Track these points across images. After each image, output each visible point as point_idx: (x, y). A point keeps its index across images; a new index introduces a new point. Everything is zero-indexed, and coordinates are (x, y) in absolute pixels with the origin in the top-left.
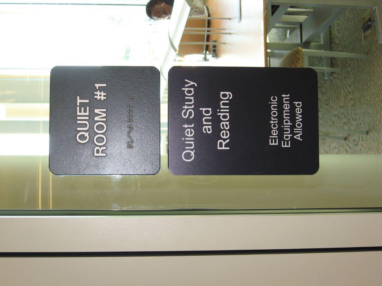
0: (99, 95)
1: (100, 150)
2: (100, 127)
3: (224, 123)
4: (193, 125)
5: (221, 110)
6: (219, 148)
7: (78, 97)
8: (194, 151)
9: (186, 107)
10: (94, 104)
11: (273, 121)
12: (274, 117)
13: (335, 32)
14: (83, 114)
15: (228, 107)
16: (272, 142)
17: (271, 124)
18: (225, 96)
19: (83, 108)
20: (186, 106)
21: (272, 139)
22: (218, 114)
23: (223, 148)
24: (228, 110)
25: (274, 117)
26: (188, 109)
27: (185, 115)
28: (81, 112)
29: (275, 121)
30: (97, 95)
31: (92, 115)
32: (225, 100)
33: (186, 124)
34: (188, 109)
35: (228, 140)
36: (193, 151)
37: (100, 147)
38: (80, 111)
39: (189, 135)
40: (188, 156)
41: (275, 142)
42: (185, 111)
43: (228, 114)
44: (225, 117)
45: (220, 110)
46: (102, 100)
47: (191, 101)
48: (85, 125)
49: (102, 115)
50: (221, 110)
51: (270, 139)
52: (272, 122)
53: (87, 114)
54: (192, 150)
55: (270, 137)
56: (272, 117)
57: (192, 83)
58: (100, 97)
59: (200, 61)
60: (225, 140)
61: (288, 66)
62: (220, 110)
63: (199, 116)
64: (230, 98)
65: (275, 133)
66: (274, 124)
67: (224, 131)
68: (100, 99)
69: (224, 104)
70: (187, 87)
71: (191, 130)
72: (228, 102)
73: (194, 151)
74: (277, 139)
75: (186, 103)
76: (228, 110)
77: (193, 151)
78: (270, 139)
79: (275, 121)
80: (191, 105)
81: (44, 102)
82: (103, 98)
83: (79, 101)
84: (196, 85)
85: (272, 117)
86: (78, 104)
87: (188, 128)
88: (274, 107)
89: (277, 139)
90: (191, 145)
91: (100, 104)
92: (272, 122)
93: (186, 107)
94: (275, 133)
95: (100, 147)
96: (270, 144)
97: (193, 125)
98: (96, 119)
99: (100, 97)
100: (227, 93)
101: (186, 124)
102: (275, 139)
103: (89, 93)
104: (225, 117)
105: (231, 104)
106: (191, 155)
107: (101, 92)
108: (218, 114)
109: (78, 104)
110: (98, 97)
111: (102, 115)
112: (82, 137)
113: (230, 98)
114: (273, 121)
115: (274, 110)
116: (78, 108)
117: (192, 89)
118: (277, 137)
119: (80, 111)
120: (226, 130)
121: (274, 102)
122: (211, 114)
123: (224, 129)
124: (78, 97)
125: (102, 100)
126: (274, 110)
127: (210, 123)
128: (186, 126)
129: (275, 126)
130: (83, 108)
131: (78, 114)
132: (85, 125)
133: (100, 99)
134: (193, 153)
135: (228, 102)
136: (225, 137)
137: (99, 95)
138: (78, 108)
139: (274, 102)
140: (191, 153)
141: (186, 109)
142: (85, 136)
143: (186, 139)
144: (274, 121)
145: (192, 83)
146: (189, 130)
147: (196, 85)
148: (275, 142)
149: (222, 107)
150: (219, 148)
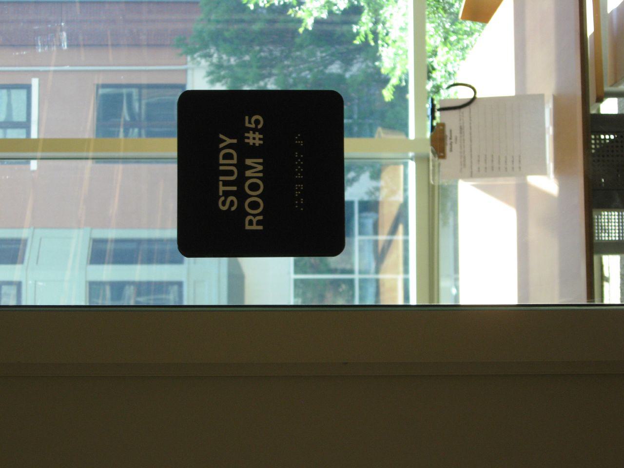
0: (257, 139)
13: (435, 102)
23: (255, 227)
28: (224, 185)
31: (242, 167)
46: (257, 145)
49: (256, 168)
59: (35, 294)
61: (619, 113)
68: (254, 144)
81: (230, 296)
82: (258, 143)
86: (221, 194)
91: (253, 151)
98: (248, 173)
107: (253, 143)
109: (221, 194)
111: (256, 168)
122: (262, 193)
125: (257, 145)
127: (221, 168)
137: (257, 139)
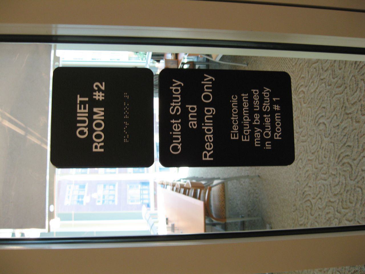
1: (99, 146)
2: (98, 125)
3: (209, 136)
4: (180, 121)
5: (206, 124)
6: (204, 159)
7: (79, 96)
8: (181, 144)
9: (173, 104)
10: (94, 103)
11: (234, 117)
12: (234, 114)
14: (82, 111)
15: (212, 121)
16: (233, 137)
17: (232, 120)
18: (208, 111)
19: (82, 106)
20: (173, 103)
21: (233, 134)
22: (203, 128)
23: (208, 159)
24: (212, 124)
25: (234, 114)
26: (175, 106)
27: (173, 110)
29: (236, 117)
30: (96, 95)
31: (91, 113)
32: (208, 115)
33: (173, 120)
34: (175, 106)
35: (212, 152)
36: (179, 144)
37: (99, 143)
38: (80, 108)
39: (177, 130)
40: (175, 149)
41: (236, 136)
42: (172, 107)
43: (211, 128)
44: (209, 130)
45: (204, 124)
47: (178, 98)
48: (84, 122)
50: (206, 124)
51: (231, 134)
52: (233, 118)
53: (87, 111)
54: (179, 143)
55: (232, 132)
56: (233, 114)
57: (179, 83)
58: (99, 94)
60: (209, 151)
62: (204, 124)
63: (185, 112)
64: (214, 113)
65: (235, 128)
66: (235, 120)
67: (209, 144)
69: (208, 119)
70: (175, 86)
71: (178, 125)
72: (211, 116)
73: (181, 144)
74: (238, 134)
75: (174, 101)
76: (212, 124)
77: (179, 144)
78: (231, 134)
79: (236, 117)
80: (178, 103)
82: (101, 98)
83: (79, 99)
84: (183, 85)
85: (233, 114)
86: (78, 102)
87: (175, 123)
88: (234, 105)
89: (238, 134)
90: (178, 139)
92: (233, 118)
93: (173, 104)
94: (235, 128)
95: (99, 143)
96: (232, 138)
97: (180, 121)
98: (95, 117)
99: (99, 94)
100: (211, 109)
101: (173, 120)
102: (236, 134)
103: (89, 92)
104: (209, 130)
105: (214, 118)
106: (178, 148)
108: (203, 128)
109: (78, 102)
110: (97, 98)
112: (82, 133)
113: (214, 113)
114: (234, 117)
115: (235, 108)
116: (78, 106)
117: (179, 88)
118: (237, 132)
119: (80, 108)
120: (210, 143)
121: (234, 100)
123: (208, 142)
124: (79, 96)
126: (235, 108)
128: (173, 121)
129: (235, 122)
130: (82, 106)
131: (78, 111)
132: (84, 122)
133: (99, 99)
134: (179, 146)
135: (211, 116)
136: (209, 149)
137: (97, 96)
138: (78, 106)
139: (234, 100)
140: (178, 146)
141: (173, 105)
142: (85, 131)
143: (174, 133)
144: (234, 117)
145: (179, 83)
146: (176, 125)
147: (183, 85)
148: (236, 136)
149: (206, 121)
150: (204, 159)
